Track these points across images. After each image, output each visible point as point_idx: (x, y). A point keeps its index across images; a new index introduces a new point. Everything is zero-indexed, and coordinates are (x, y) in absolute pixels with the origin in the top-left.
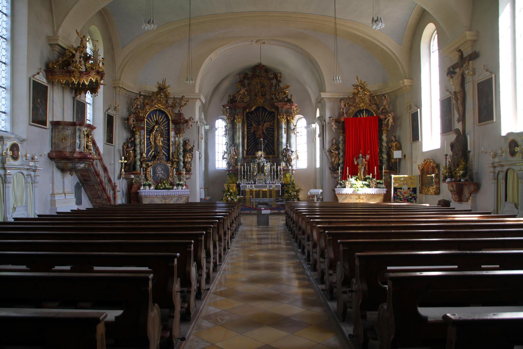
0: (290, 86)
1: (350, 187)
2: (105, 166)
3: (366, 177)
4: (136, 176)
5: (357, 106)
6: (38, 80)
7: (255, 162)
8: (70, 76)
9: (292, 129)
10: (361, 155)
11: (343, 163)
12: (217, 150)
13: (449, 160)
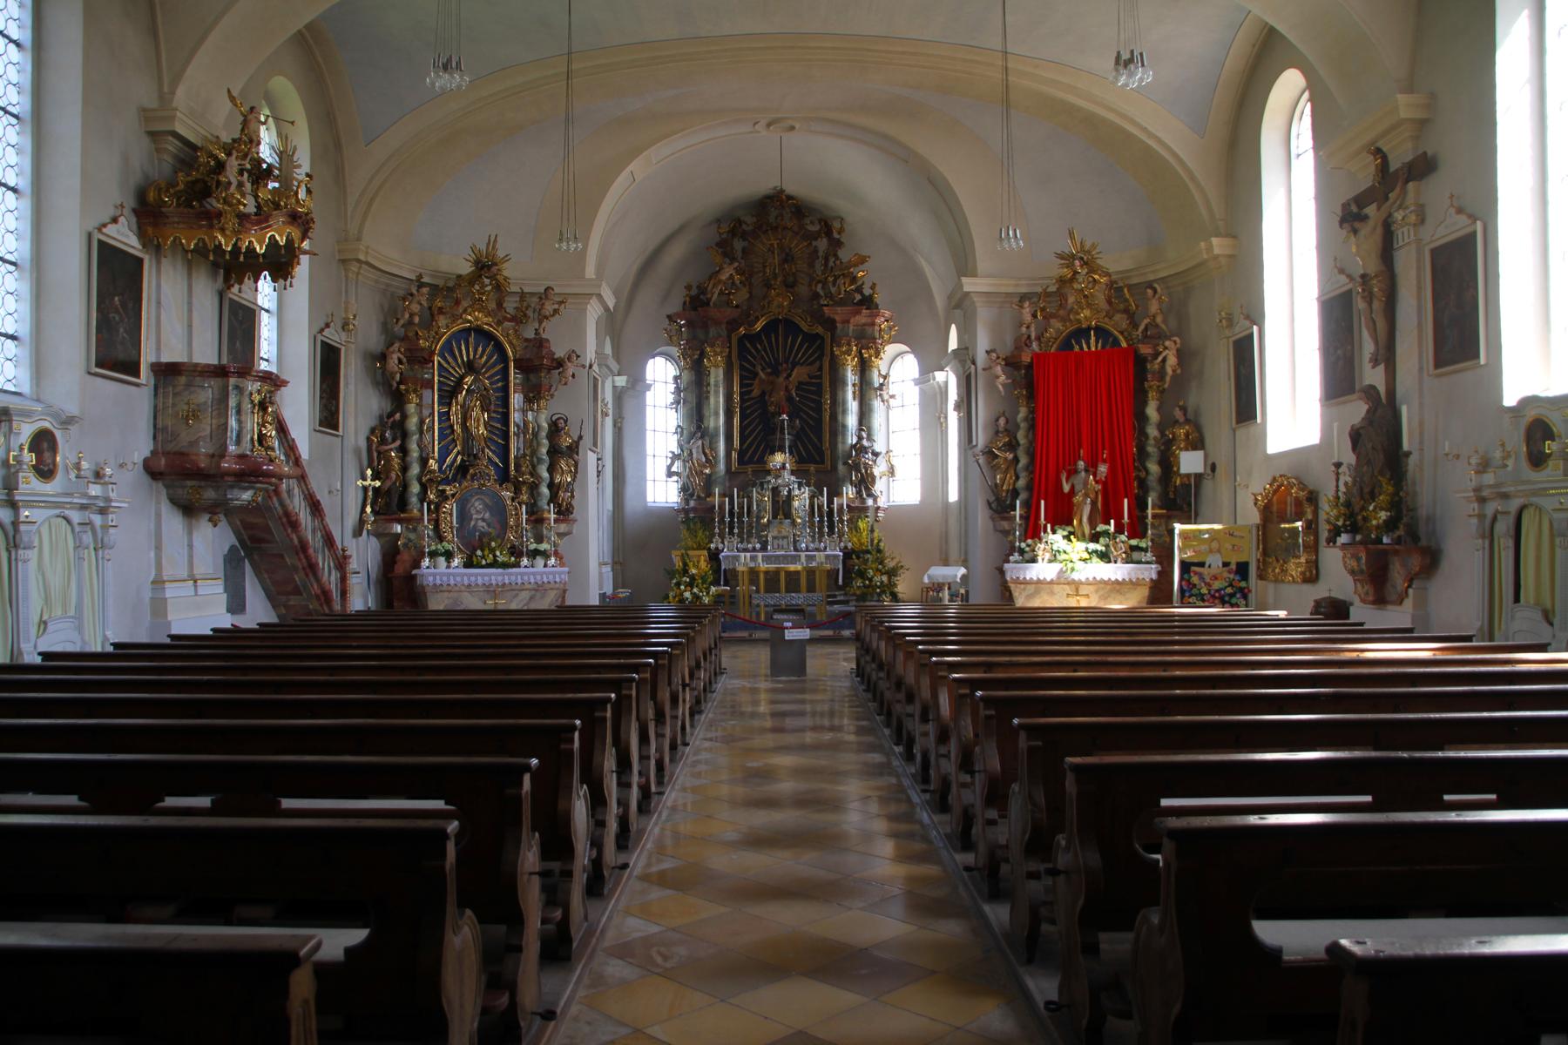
0: (869, 257)
1: (1050, 561)
2: (315, 496)
3: (1098, 529)
4: (407, 528)
5: (1071, 317)
6: (114, 239)
7: (765, 486)
8: (211, 227)
9: (876, 385)
10: (1081, 464)
11: (1029, 488)
12: (649, 450)
13: (1346, 478)
